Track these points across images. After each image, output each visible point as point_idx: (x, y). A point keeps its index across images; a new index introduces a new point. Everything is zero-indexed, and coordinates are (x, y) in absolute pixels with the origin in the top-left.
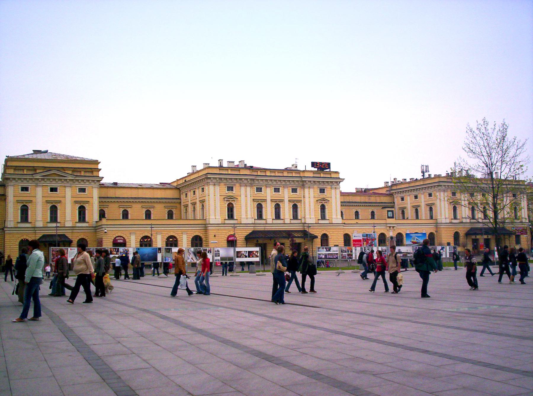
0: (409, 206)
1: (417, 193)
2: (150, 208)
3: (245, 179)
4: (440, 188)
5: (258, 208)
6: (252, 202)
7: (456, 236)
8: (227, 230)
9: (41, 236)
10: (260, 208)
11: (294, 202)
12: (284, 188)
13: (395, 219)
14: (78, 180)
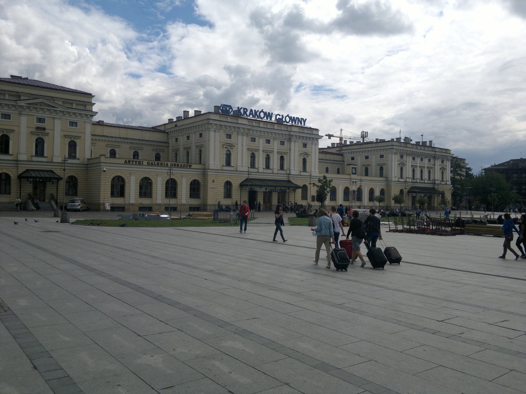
0: (374, 164)
1: (369, 154)
2: (137, 149)
3: (215, 124)
4: (392, 150)
5: (251, 157)
6: (247, 151)
7: (228, 185)
8: (225, 176)
9: (245, 179)
10: (253, 157)
11: (281, 154)
12: (243, 136)
13: (358, 175)
14: (69, 113)
